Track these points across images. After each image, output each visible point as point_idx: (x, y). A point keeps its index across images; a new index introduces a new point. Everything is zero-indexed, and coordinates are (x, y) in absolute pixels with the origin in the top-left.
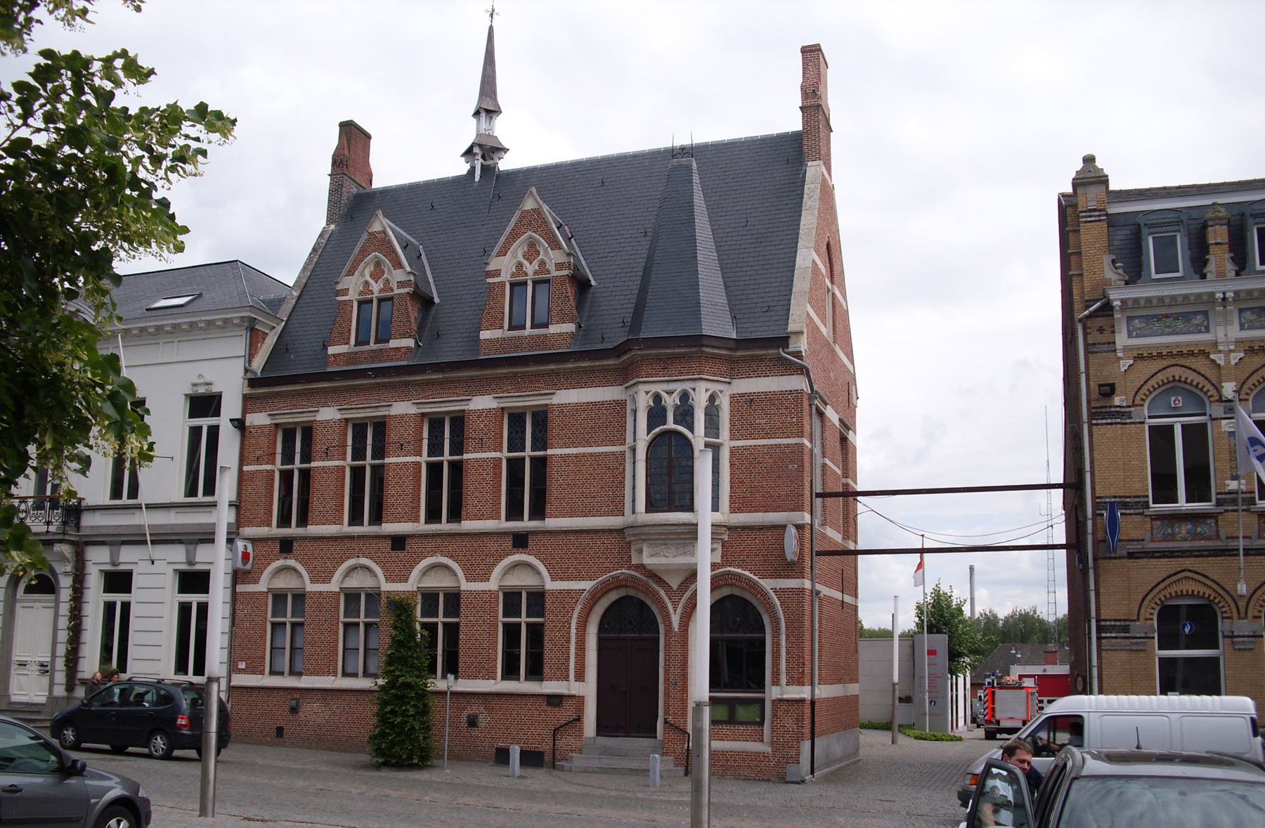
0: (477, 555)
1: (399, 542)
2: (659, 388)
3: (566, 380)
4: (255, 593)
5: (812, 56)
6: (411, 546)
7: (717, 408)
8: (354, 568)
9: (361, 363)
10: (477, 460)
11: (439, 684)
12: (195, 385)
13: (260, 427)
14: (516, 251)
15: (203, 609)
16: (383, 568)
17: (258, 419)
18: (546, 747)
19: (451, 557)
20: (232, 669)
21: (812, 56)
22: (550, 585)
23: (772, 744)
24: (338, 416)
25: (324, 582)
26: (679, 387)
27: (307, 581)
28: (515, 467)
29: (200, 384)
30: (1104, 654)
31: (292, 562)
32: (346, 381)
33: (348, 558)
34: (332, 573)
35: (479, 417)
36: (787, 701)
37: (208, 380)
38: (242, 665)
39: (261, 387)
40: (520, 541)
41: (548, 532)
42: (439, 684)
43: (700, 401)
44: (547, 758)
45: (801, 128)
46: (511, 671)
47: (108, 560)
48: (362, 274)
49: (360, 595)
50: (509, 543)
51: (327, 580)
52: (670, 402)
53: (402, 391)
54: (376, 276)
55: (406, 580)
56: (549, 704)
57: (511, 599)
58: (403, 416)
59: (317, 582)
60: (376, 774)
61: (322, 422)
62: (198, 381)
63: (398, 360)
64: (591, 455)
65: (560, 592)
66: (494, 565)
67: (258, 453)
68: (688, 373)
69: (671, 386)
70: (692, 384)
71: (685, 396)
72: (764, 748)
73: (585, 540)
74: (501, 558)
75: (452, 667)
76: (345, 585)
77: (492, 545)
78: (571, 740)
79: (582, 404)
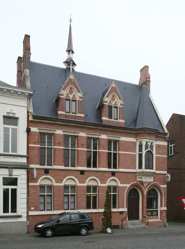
0: (103, 176)
1: (82, 172)
2: (148, 140)
3: (107, 132)
4: (36, 186)
5: (27, 37)
6: (86, 173)
7: (148, 145)
8: (44, 179)
9: (70, 118)
10: (103, 152)
11: (114, 210)
12: (9, 113)
13: (35, 132)
14: (67, 90)
15: (14, 192)
16: (78, 179)
17: (34, 129)
18: (120, 224)
19: (97, 177)
20: (29, 209)
21: (27, 37)
22: (120, 185)
23: (161, 219)
24: (62, 133)
25: (60, 183)
26: (151, 141)
27: (99, 182)
28: (109, 154)
29: (11, 113)
30: (43, 202)
31: (49, 176)
32: (67, 123)
33: (67, 176)
34: (62, 180)
35: (58, 136)
36: (164, 210)
37: (13, 112)
38: (33, 208)
39: (35, 119)
40: (113, 174)
41: (119, 172)
42: (114, 210)
43: (144, 144)
44: (120, 227)
45: (31, 61)
46: (88, 207)
47: (8, 174)
48: (67, 91)
49: (45, 187)
50: (111, 174)
51: (61, 182)
52: (149, 144)
53: (61, 126)
54: (71, 92)
55: (85, 183)
56: (120, 214)
57: (89, 188)
58: (82, 137)
59: (58, 183)
60: (37, 239)
61: (57, 134)
62: (11, 112)
63: (81, 120)
64: (129, 154)
65: (122, 187)
66: (107, 180)
67: (34, 141)
68: (153, 138)
69: (150, 140)
70: (141, 140)
71: (141, 143)
72: (159, 220)
73: (128, 174)
74: (109, 178)
75: (115, 207)
76: (65, 184)
77: (107, 175)
78: (125, 222)
79: (126, 141)
